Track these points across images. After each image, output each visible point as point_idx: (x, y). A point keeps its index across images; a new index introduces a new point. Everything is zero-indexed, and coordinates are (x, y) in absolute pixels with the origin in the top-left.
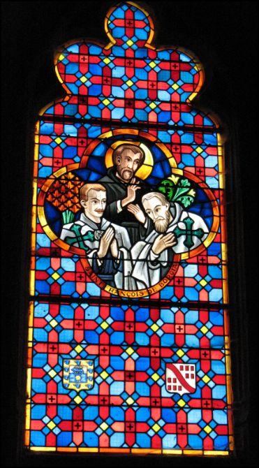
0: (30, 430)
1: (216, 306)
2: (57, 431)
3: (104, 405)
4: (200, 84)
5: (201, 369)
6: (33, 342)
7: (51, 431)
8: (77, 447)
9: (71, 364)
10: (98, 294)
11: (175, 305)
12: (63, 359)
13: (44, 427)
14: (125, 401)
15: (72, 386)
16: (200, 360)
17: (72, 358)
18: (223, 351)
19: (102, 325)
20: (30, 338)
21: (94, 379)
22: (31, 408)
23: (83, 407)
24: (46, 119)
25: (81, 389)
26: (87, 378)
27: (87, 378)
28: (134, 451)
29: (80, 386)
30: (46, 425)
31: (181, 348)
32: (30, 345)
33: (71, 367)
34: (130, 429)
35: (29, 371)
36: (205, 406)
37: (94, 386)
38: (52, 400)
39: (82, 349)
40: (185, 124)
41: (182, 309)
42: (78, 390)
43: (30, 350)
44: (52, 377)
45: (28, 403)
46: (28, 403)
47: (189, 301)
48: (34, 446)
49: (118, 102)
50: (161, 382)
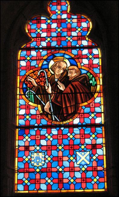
0: (104, 182)
1: (99, 125)
2: (52, 183)
3: (95, 171)
4: (91, 27)
5: (47, 155)
6: (18, 146)
7: (93, 180)
8: (38, 190)
9: (39, 155)
10: (46, 124)
11: (36, 127)
12: (31, 153)
13: (69, 181)
14: (81, 169)
15: (35, 164)
16: (74, 150)
17: (35, 152)
18: (102, 145)
19: (71, 138)
20: (17, 145)
21: (45, 161)
22: (18, 174)
23: (63, 173)
24: (23, 49)
25: (39, 165)
26: (42, 160)
27: (42, 160)
28: (62, 191)
29: (39, 164)
30: (95, 178)
31: (83, 145)
32: (17, 147)
33: (35, 156)
34: (84, 179)
35: (17, 159)
36: (94, 170)
37: (45, 164)
38: (26, 170)
39: (84, 147)
40: (63, 46)
41: (39, 129)
42: (38, 166)
43: (17, 150)
44: (72, 160)
45: (16, 172)
46: (16, 172)
47: (43, 125)
48: (105, 187)
49: (53, 39)
50: (74, 160)
